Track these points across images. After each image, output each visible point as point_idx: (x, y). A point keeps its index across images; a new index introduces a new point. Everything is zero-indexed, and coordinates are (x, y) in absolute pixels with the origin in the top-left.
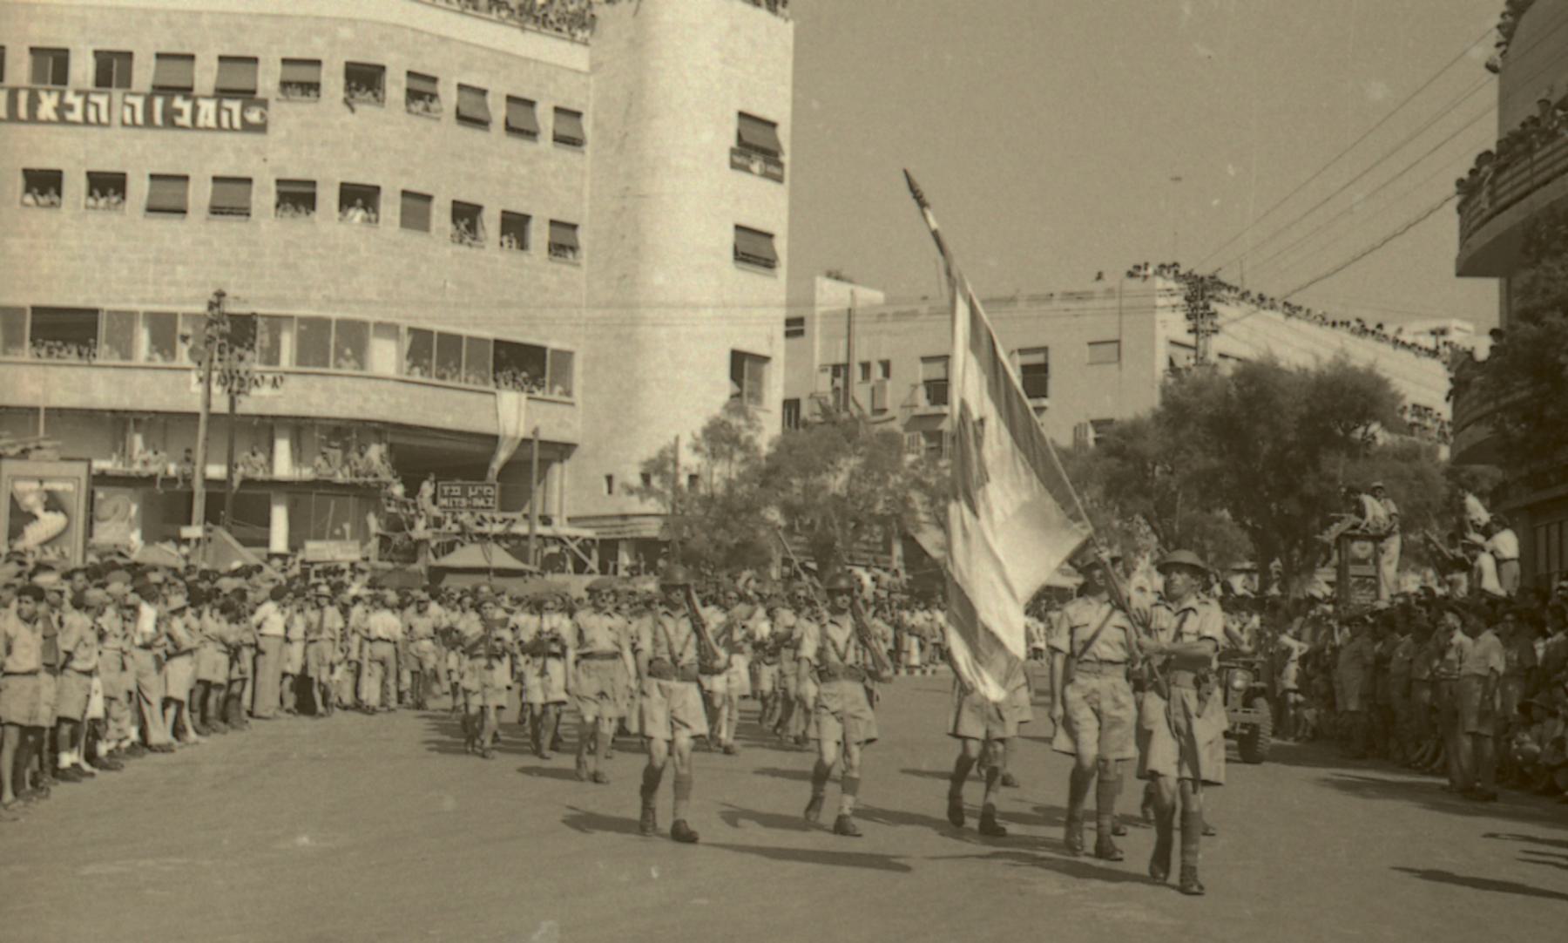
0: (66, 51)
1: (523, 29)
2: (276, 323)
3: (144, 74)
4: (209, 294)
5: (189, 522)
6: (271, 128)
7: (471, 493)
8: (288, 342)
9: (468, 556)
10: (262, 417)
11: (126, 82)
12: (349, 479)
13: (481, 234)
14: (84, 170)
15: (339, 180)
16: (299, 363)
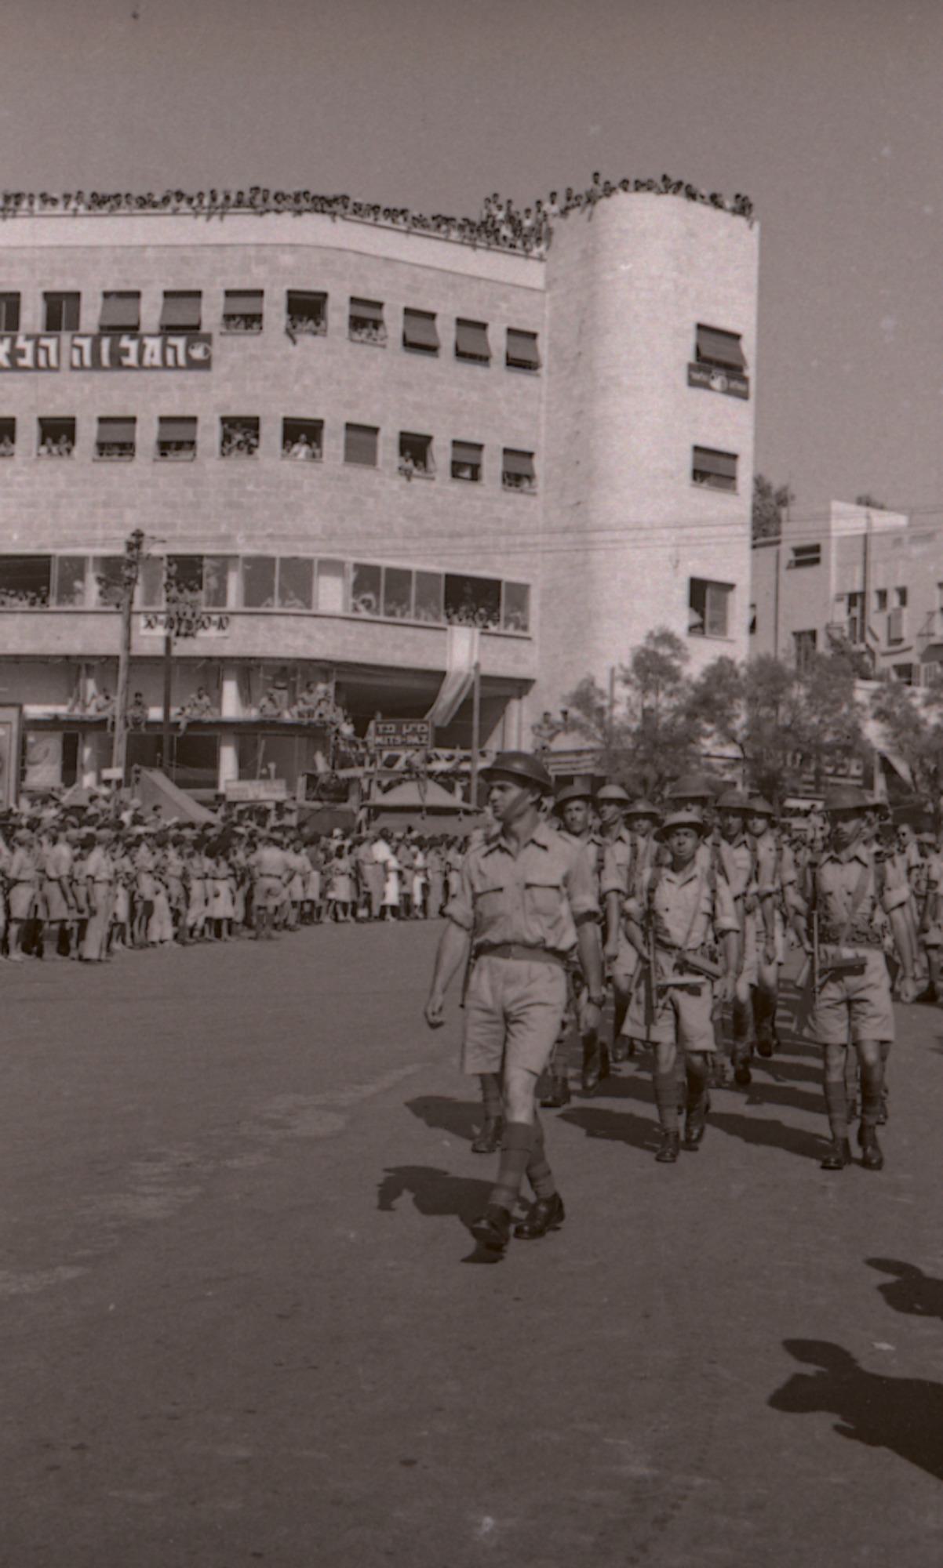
0: (18, 295)
1: (474, 247)
2: (224, 563)
3: (90, 316)
4: (126, 535)
5: (109, 766)
6: (214, 364)
7: (405, 731)
8: (234, 584)
9: (407, 794)
10: (210, 658)
11: (74, 325)
12: (296, 719)
13: (431, 466)
14: (35, 416)
15: (282, 414)
16: (247, 603)
